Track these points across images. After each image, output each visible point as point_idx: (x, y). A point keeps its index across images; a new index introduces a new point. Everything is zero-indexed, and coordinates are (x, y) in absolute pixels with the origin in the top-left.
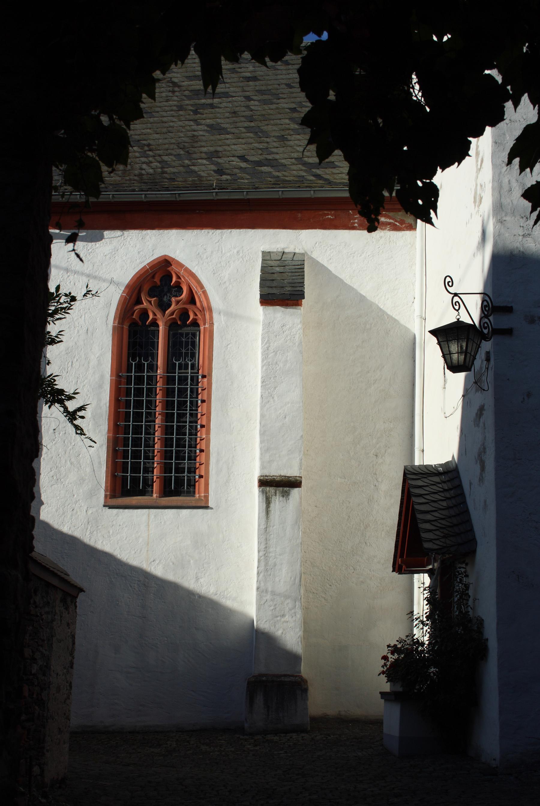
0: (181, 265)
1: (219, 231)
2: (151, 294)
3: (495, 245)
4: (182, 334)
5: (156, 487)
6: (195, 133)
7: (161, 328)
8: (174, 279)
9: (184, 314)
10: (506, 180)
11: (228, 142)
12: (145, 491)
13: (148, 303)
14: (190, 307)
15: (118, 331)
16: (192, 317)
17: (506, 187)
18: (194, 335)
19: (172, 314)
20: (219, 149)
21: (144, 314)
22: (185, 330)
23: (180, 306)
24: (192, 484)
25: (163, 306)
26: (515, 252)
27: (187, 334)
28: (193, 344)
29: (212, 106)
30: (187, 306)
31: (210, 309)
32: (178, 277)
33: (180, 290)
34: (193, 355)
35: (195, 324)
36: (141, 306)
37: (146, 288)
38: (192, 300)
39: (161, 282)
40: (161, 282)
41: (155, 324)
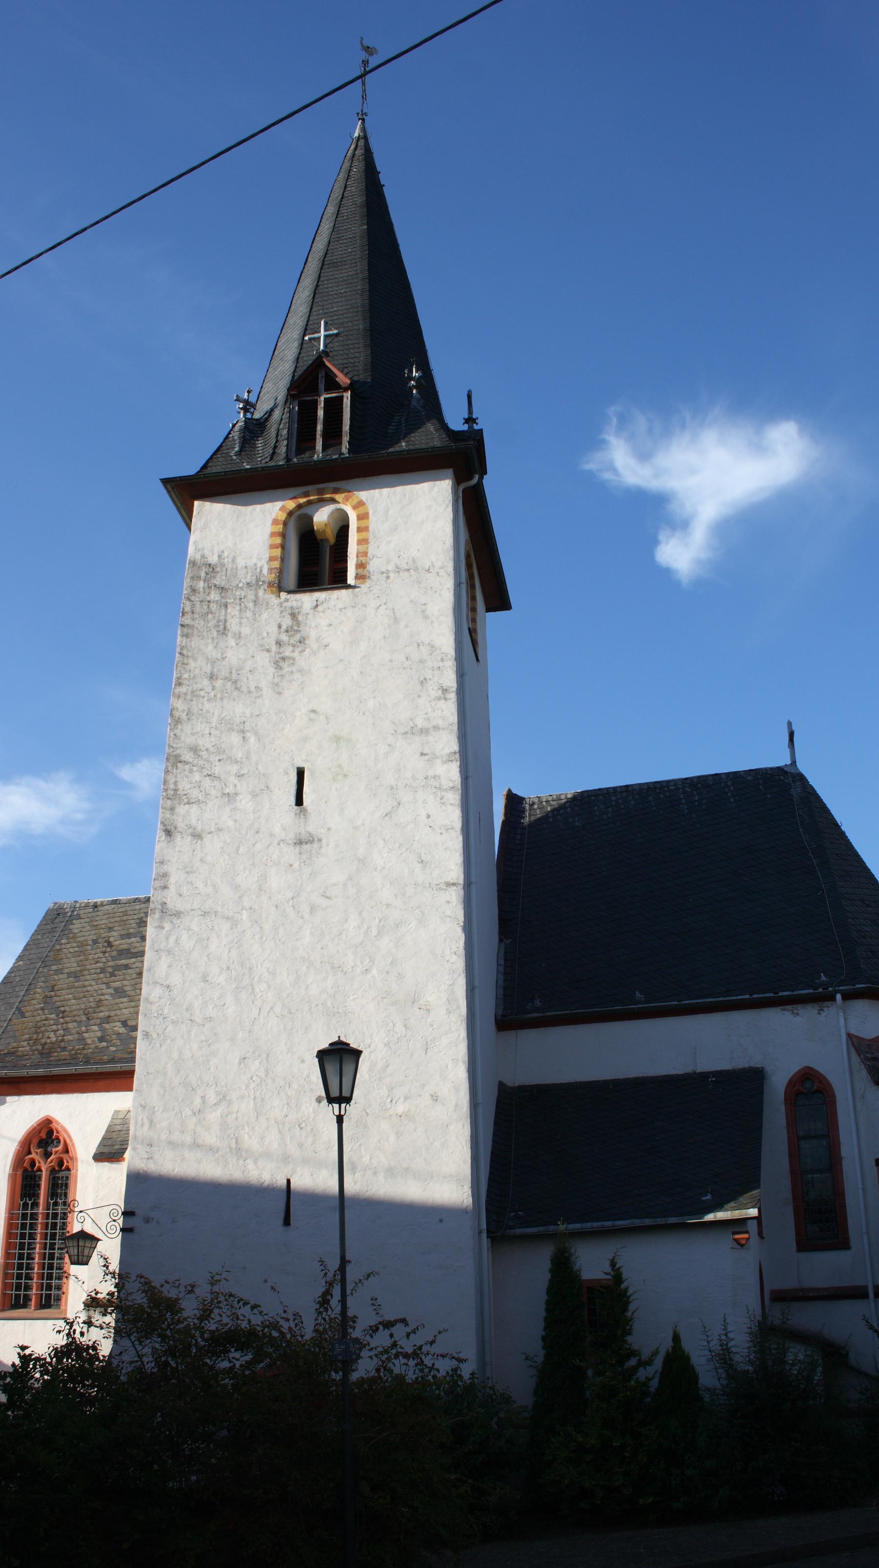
0: (58, 1123)
1: (85, 1095)
2: (39, 1147)
3: (129, 1165)
4: (58, 1178)
5: (33, 1303)
6: (102, 997)
7: (44, 1173)
8: (55, 1134)
9: (61, 1162)
10: (140, 1118)
11: (122, 1006)
12: (25, 1306)
13: (36, 1155)
14: (65, 1156)
15: (13, 1177)
16: (65, 1164)
17: (140, 1124)
18: (67, 1178)
19: (51, 1162)
20: (113, 1013)
21: (33, 1163)
22: (61, 1174)
23: (57, 1155)
24: (58, 1299)
25: (47, 1155)
26: (141, 1171)
27: (63, 1177)
28: (67, 1185)
29: (127, 967)
30: (62, 1155)
31: (77, 1159)
32: (58, 1132)
33: (59, 1142)
34: (66, 1195)
35: (68, 1169)
36: (30, 1156)
37: (35, 1141)
38: (66, 1150)
39: (45, 1137)
40: (45, 1137)
41: (40, 1170)
